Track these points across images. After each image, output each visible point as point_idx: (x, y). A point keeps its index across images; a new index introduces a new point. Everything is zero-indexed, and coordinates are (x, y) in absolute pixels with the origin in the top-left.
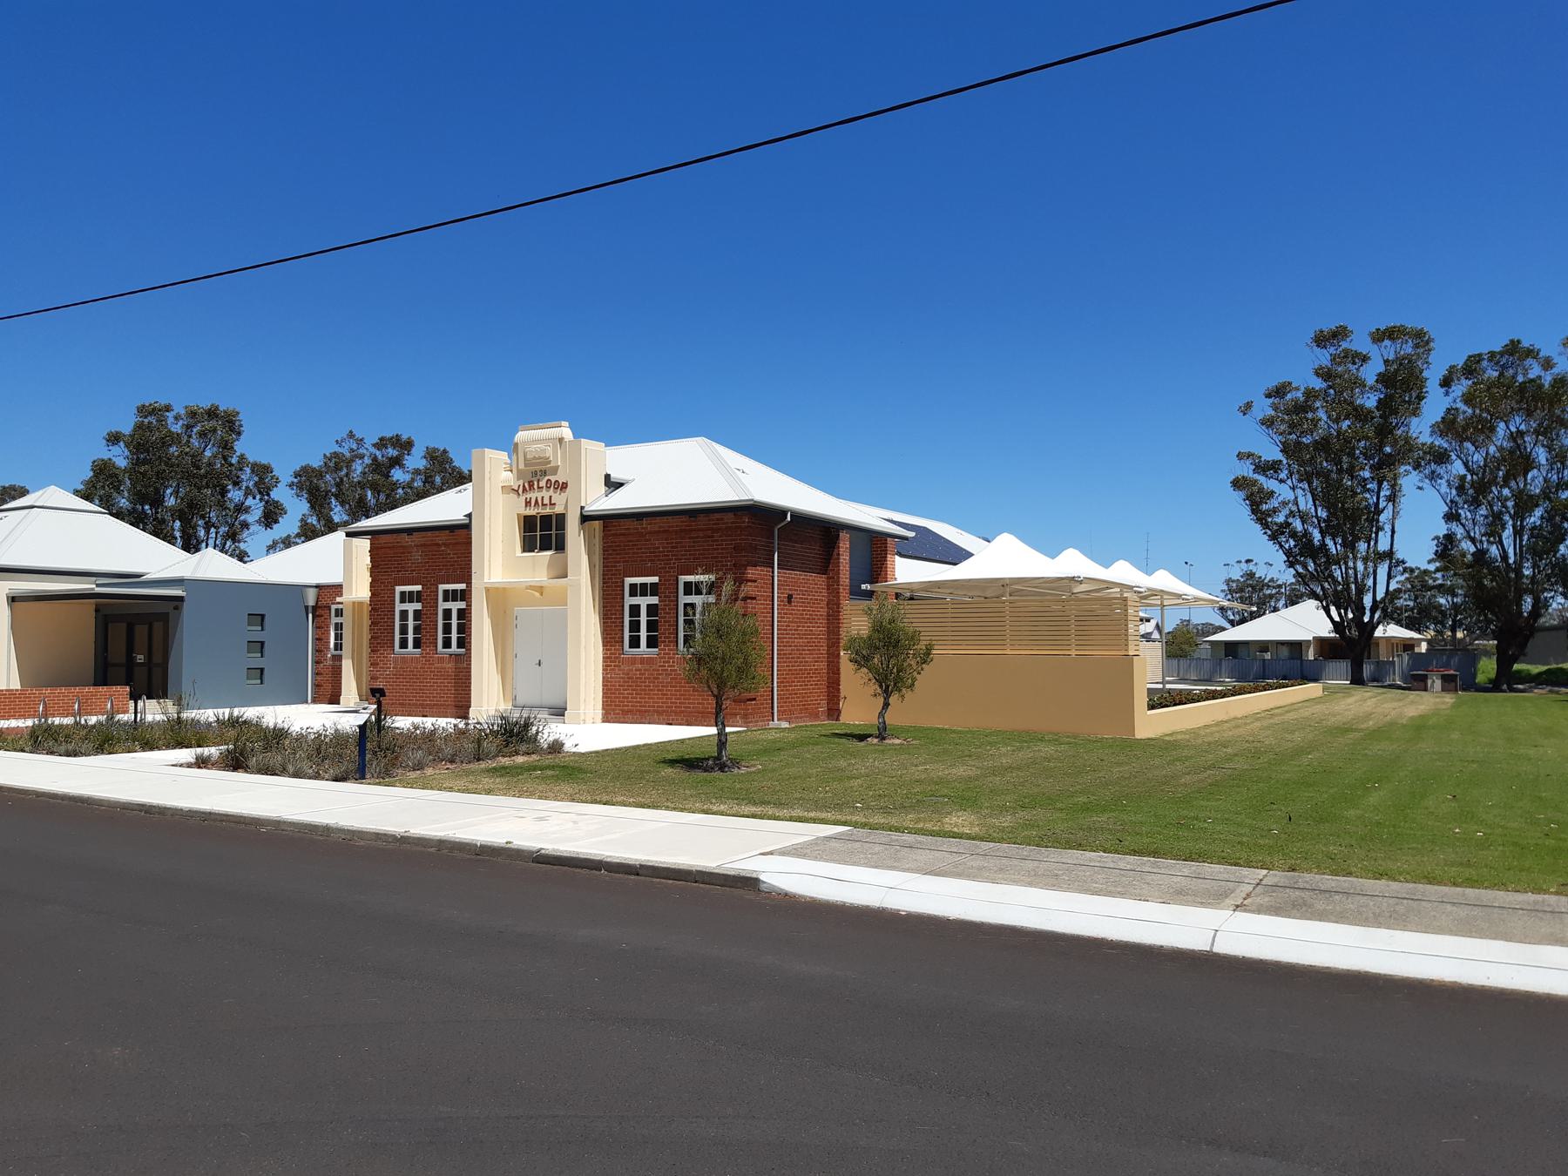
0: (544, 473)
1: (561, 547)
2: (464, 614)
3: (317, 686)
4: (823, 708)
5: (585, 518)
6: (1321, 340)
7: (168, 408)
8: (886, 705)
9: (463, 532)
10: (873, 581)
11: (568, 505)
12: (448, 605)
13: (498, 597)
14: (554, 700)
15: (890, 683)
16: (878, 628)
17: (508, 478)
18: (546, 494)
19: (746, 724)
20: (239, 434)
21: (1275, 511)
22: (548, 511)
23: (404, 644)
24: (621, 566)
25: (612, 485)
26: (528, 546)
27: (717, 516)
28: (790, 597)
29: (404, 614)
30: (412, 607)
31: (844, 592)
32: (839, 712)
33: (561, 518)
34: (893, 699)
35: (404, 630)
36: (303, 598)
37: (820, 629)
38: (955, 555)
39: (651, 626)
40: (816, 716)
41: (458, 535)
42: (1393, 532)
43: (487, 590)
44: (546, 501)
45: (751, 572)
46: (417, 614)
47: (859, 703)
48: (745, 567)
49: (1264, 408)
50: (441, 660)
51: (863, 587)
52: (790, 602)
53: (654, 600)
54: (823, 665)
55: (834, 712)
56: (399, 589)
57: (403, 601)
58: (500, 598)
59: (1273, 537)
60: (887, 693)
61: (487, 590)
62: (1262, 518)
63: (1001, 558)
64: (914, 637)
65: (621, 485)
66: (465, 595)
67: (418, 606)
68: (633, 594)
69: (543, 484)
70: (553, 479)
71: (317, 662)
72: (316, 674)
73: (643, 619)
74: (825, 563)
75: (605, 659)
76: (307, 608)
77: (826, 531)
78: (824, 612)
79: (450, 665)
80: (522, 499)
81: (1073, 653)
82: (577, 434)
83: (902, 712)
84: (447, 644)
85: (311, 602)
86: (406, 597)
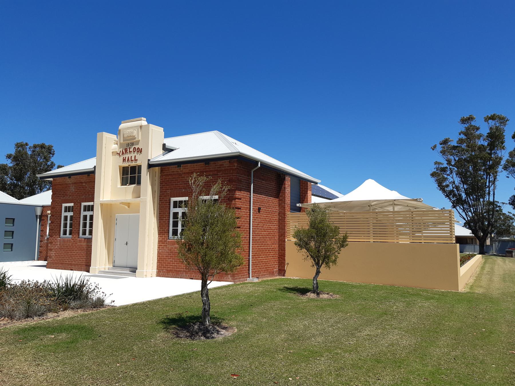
0: (133, 144)
1: (139, 183)
2: (92, 217)
3: (40, 252)
4: (276, 270)
5: (150, 166)
6: (464, 121)
7: (27, 144)
8: (318, 273)
10: (302, 202)
11: (142, 161)
13: (107, 208)
14: (131, 264)
15: (321, 258)
16: (313, 225)
17: (115, 147)
18: (133, 155)
19: (234, 280)
20: (53, 154)
21: (447, 186)
22: (133, 164)
23: (65, 233)
24: (169, 192)
25: (167, 150)
26: (124, 182)
27: (220, 163)
28: (259, 209)
29: (66, 217)
30: (70, 214)
31: (288, 208)
32: (284, 271)
33: (140, 167)
34: (323, 269)
35: (65, 226)
36: (35, 211)
37: (275, 227)
38: (330, 197)
40: (272, 274)
41: (89, 176)
42: (494, 194)
43: (102, 205)
44: (133, 159)
45: (238, 194)
46: (71, 217)
47: (299, 267)
48: (235, 191)
49: (439, 148)
51: (298, 205)
52: (259, 211)
54: (276, 246)
55: (282, 271)
57: (65, 211)
58: (108, 209)
59: (447, 196)
60: (318, 264)
61: (102, 205)
62: (442, 188)
63: (370, 191)
64: (336, 231)
65: (172, 150)
66: (91, 208)
67: (71, 214)
68: (175, 206)
69: (132, 150)
70: (137, 147)
71: (41, 241)
72: (40, 246)
74: (278, 192)
75: (159, 242)
76: (37, 216)
77: (280, 175)
78: (277, 218)
79: (84, 244)
81: (372, 241)
82: (149, 122)
83: (327, 275)
85: (39, 213)
86: (68, 209)
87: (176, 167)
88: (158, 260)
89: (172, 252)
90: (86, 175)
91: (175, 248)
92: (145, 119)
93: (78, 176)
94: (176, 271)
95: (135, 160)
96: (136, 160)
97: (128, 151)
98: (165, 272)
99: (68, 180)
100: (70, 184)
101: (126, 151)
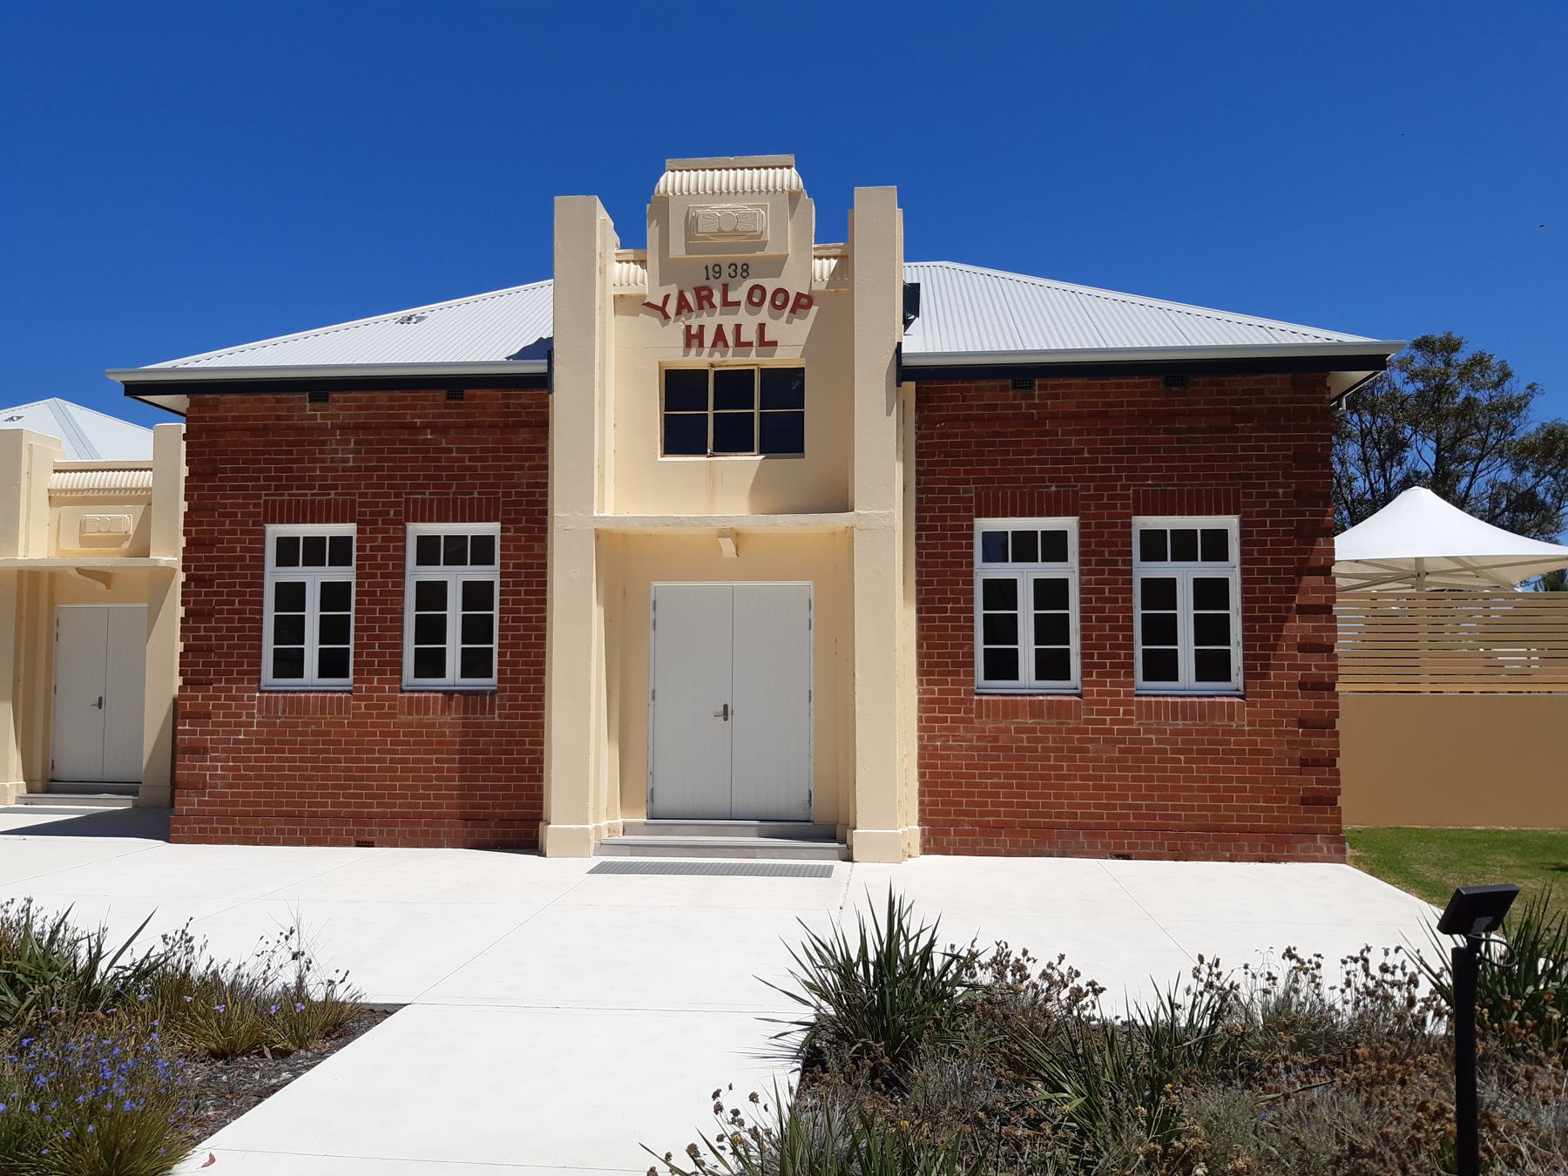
0: (745, 270)
9: (526, 396)
12: (291, 575)
24: (971, 491)
39: (332, 630)
44: (749, 334)
50: (418, 705)
53: (344, 574)
56: (275, 531)
69: (739, 294)
73: (312, 614)
80: (676, 329)
81: (1426, 688)
84: (430, 664)
87: (1004, 389)
88: (922, 784)
89: (1008, 749)
90: (441, 395)
91: (1018, 730)
92: (662, 179)
93: (382, 397)
94: (1036, 826)
95: (762, 342)
96: (766, 344)
97: (717, 298)
98: (972, 833)
99: (309, 411)
100: (322, 429)
101: (703, 296)
